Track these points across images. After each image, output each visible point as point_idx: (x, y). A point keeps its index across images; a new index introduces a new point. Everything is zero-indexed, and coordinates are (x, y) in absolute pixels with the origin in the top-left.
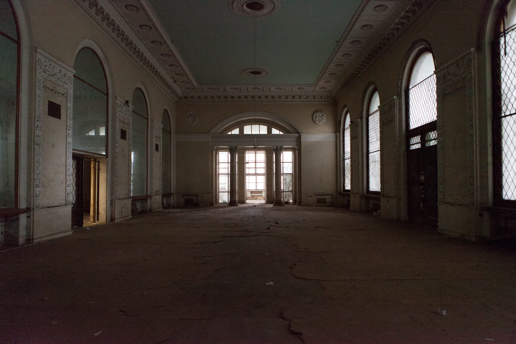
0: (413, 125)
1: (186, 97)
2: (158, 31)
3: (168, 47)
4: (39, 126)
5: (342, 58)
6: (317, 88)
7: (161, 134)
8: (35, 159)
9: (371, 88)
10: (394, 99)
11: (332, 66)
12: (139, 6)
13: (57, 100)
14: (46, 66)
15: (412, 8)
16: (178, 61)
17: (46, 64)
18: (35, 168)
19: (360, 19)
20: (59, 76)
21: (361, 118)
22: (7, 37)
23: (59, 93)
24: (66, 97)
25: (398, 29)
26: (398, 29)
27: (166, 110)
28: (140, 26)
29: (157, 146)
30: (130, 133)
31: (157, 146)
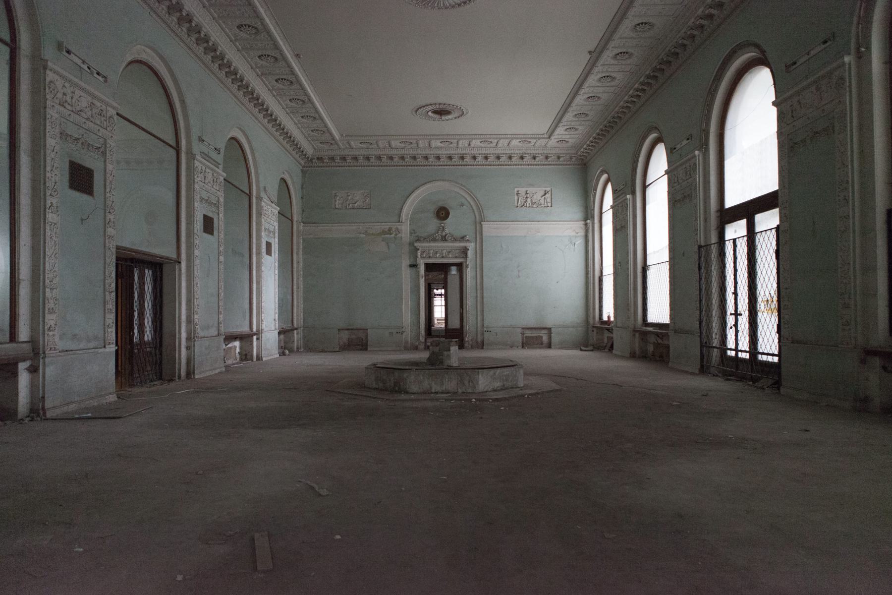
0: (730, 202)
1: (320, 159)
2: (270, 36)
3: (289, 66)
4: (55, 205)
5: (613, 62)
6: (553, 142)
7: (276, 224)
8: (47, 265)
9: (653, 136)
10: (695, 156)
11: (580, 99)
12: (260, 27)
13: (89, 161)
14: (64, 94)
15: (707, 12)
16: (326, 126)
17: (65, 90)
18: (47, 281)
19: (631, 13)
20: (89, 113)
21: (633, 193)
22: (164, 142)
23: (67, 135)
24: (104, 154)
25: (702, 26)
26: (710, 16)
27: (283, 180)
28: (260, 57)
29: (269, 245)
30: (220, 222)
31: (269, 245)
